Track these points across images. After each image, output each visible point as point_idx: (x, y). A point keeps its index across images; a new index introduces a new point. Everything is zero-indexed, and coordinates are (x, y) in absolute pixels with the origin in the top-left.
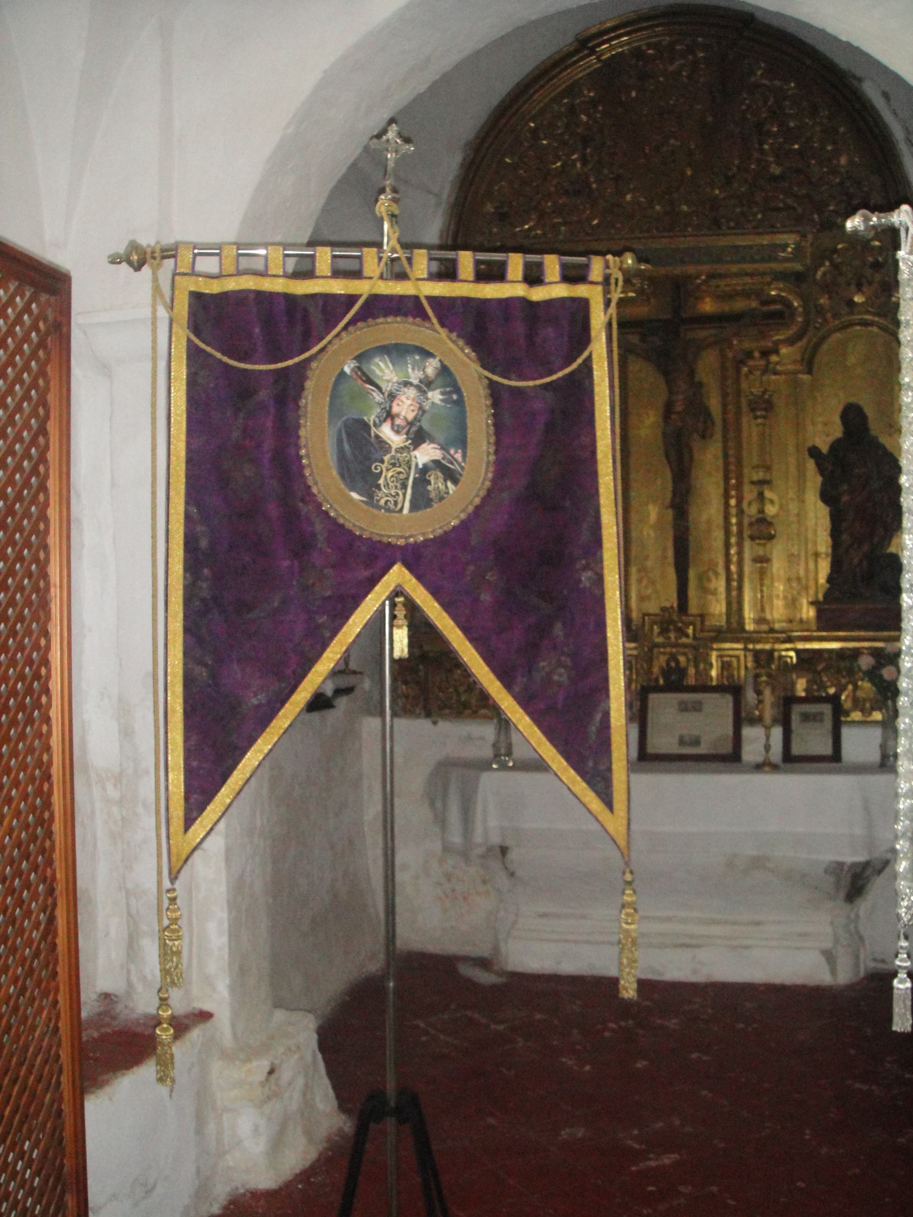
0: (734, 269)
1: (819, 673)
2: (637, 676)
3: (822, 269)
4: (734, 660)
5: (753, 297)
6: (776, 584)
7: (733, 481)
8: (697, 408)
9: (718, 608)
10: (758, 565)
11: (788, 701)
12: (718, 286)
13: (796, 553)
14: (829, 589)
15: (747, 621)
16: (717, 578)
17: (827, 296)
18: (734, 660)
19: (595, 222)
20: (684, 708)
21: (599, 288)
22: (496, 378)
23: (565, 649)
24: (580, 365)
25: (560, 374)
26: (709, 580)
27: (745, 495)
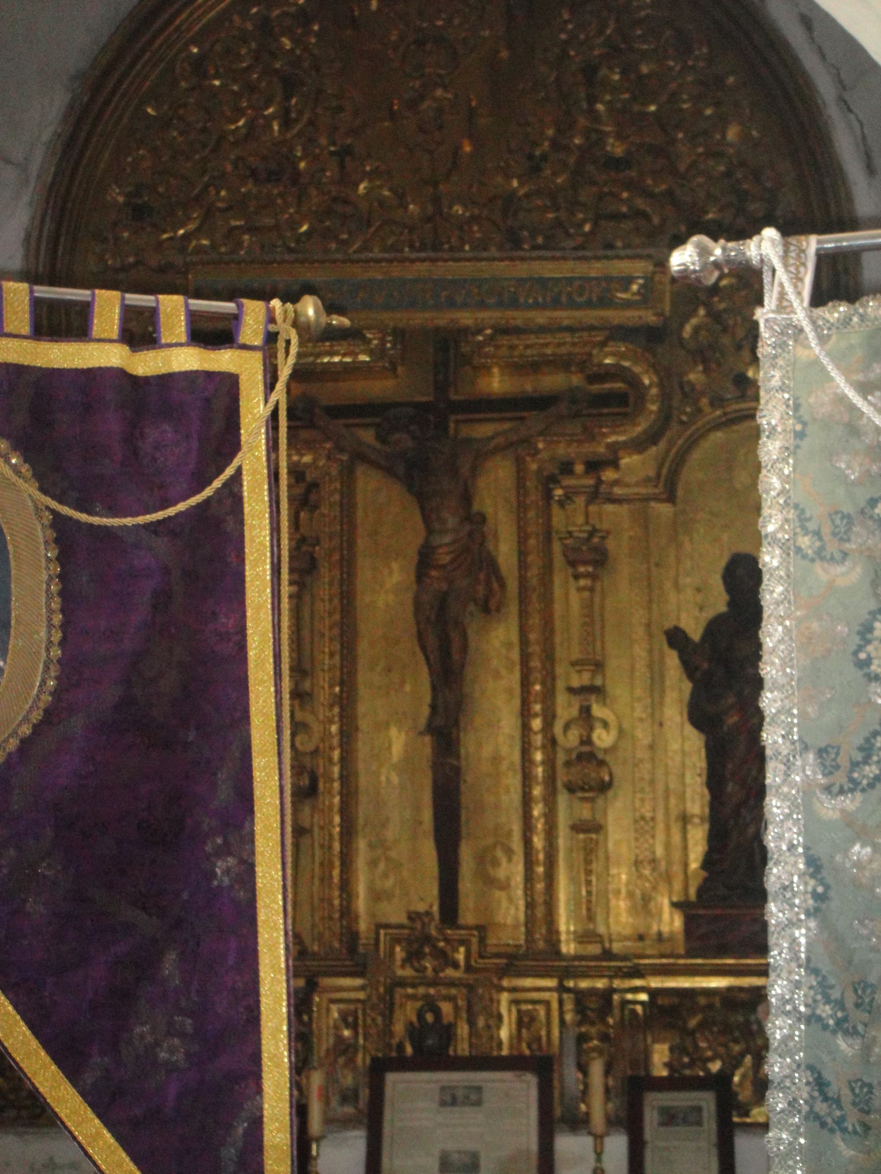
0: (541, 318)
1: (692, 1033)
2: (365, 1039)
3: (694, 321)
4: (542, 1012)
5: (573, 369)
6: (613, 871)
7: (538, 687)
8: (477, 558)
9: (510, 911)
10: (582, 836)
11: (634, 1088)
12: (512, 348)
13: (648, 815)
14: (706, 880)
15: (563, 937)
16: (510, 860)
17: (700, 368)
18: (542, 1012)
19: (305, 228)
20: (450, 1099)
21: (259, 355)
22: (66, 510)
23: (183, 1003)
24: (218, 491)
25: (182, 507)
26: (496, 863)
27: (559, 711)
